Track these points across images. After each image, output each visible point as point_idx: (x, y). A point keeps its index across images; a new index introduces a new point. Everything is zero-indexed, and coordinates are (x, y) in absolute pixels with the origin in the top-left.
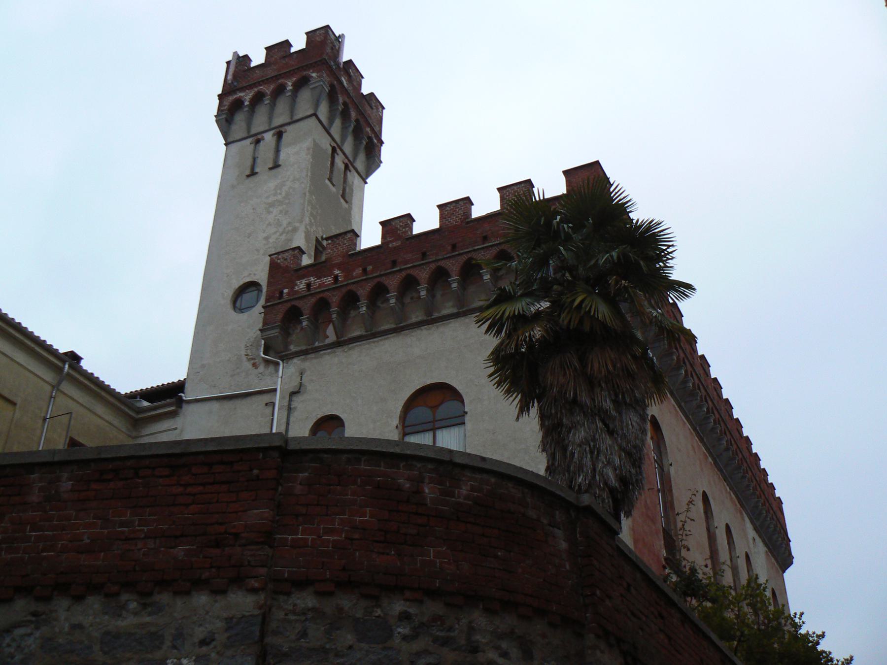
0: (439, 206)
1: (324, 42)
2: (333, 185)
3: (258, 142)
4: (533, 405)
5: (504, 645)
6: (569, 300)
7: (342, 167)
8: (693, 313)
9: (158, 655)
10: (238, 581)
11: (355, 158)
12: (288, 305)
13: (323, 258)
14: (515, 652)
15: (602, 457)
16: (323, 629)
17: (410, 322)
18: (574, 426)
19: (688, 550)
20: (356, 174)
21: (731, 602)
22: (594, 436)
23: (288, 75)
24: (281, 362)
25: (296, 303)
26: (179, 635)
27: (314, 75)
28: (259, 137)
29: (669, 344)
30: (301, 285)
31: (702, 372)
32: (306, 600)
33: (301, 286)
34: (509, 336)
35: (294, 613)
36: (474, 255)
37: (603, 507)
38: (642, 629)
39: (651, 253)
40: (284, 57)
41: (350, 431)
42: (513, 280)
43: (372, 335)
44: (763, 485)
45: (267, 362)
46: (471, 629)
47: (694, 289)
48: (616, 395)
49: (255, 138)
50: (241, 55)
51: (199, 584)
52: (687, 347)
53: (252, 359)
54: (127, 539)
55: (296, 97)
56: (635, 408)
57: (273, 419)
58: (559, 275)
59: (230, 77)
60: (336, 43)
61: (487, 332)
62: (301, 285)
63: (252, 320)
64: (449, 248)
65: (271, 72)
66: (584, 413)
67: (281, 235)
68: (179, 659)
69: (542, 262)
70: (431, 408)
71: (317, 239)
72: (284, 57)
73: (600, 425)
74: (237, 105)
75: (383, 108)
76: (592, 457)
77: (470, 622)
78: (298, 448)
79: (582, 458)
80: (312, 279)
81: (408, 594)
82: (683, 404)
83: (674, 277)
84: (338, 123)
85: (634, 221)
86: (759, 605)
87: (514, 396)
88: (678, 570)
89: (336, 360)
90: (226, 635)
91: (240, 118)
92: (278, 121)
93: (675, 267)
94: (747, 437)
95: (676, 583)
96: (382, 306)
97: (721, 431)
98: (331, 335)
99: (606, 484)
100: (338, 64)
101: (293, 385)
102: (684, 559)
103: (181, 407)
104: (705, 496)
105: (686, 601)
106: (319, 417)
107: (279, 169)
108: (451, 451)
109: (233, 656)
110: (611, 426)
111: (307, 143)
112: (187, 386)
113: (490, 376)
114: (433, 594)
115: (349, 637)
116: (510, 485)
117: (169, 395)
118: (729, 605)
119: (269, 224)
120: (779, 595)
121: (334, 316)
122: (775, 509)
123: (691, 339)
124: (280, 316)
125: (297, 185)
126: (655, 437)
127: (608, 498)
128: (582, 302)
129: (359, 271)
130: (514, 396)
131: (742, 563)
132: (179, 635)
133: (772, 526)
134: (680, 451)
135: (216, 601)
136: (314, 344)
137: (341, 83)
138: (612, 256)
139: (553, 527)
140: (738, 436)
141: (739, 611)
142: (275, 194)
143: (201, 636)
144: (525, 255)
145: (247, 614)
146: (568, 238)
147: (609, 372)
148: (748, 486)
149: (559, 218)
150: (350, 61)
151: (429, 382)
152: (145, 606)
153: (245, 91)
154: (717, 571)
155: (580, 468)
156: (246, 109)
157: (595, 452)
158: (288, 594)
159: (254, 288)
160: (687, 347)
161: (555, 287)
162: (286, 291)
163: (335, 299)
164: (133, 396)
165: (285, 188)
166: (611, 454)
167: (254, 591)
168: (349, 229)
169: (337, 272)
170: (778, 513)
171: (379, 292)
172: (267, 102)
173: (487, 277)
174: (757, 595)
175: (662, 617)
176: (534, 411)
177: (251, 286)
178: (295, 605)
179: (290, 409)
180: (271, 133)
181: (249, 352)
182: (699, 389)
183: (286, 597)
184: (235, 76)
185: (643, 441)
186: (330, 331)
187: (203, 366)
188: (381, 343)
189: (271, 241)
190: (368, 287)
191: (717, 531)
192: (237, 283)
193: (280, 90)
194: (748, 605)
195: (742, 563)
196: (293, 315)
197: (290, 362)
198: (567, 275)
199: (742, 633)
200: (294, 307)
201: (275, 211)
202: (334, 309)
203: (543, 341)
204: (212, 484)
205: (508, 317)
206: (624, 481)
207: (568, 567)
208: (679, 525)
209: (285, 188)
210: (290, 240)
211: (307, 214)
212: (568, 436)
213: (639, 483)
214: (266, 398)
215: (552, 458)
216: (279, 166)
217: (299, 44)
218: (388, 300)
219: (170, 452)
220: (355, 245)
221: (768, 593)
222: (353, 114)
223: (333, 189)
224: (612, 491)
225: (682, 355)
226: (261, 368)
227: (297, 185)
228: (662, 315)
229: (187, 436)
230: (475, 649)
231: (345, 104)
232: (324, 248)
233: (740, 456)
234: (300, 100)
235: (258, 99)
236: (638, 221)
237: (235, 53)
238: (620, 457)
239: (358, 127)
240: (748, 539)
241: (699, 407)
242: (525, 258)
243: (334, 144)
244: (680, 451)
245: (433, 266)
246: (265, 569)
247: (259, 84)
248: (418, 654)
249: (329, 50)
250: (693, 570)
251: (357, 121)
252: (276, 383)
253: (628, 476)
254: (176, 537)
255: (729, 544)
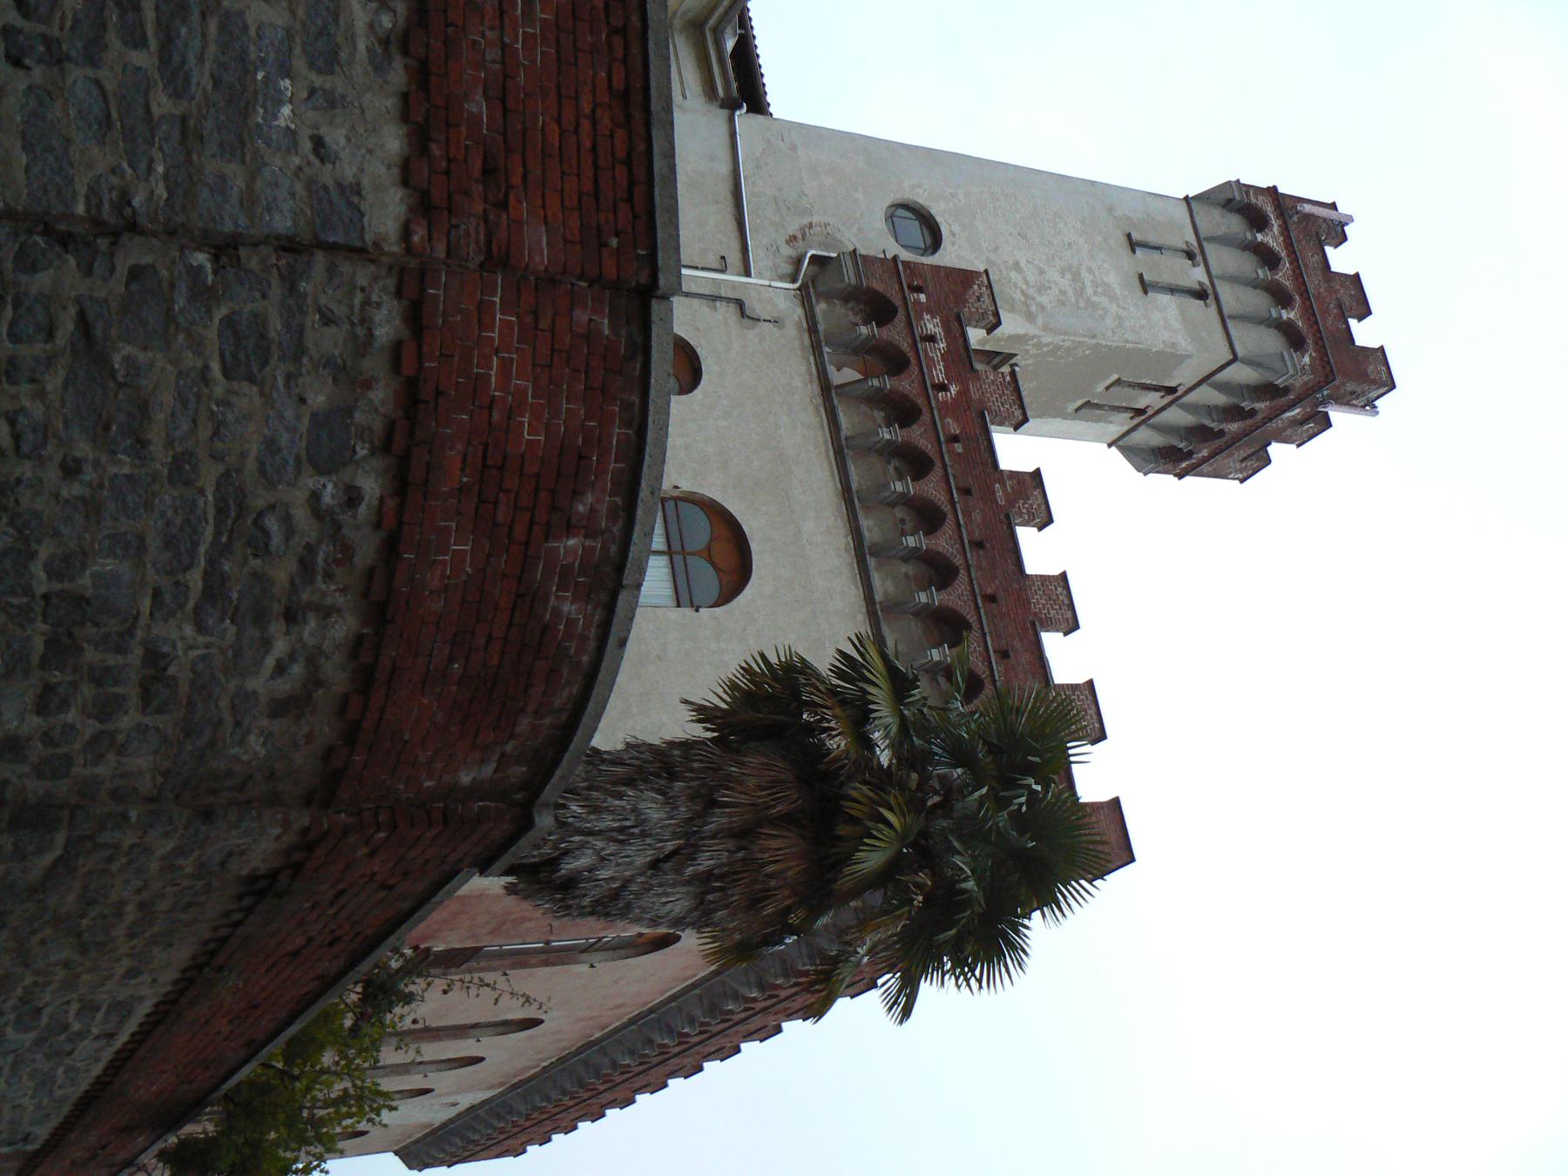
0: (1064, 575)
1: (1365, 378)
2: (1107, 388)
3: (1190, 255)
4: (708, 729)
5: (297, 669)
6: (892, 801)
7: (1140, 405)
8: (859, 1014)
9: (299, 64)
10: (424, 206)
11: (1155, 427)
12: (898, 302)
13: (978, 366)
14: (283, 687)
15: (613, 848)
16: (337, 352)
17: (861, 515)
18: (669, 801)
19: (445, 992)
20: (1126, 428)
21: (350, 1061)
22: (649, 835)
23: (1308, 312)
24: (797, 285)
25: (901, 315)
26: (332, 102)
27: (1307, 359)
28: (1199, 258)
29: (806, 974)
30: (932, 325)
31: (753, 1027)
32: (387, 325)
33: (930, 326)
34: (833, 692)
35: (366, 303)
36: (976, 633)
37: (524, 851)
38: (313, 907)
39: (969, 949)
40: (1340, 306)
41: (678, 404)
42: (929, 702)
43: (840, 450)
44: (549, 1125)
45: (798, 262)
46: (326, 612)
47: (901, 1022)
48: (721, 877)
49: (1197, 251)
50: (1346, 229)
51: (420, 137)
52: (799, 1002)
53: (804, 236)
54: (502, 13)
55: (1269, 326)
56: (696, 908)
57: (696, 268)
58: (936, 784)
59: (1307, 208)
60: (1362, 401)
61: (841, 652)
62: (932, 325)
63: (874, 237)
64: (989, 591)
65: (1314, 282)
66: (692, 819)
67: (1023, 292)
68: (291, 101)
69: (960, 754)
70: (709, 548)
71: (1013, 355)
72: (1340, 306)
73: (670, 846)
74: (1257, 220)
75: (1242, 481)
76: (613, 830)
77: (339, 611)
78: (654, 317)
79: (613, 813)
80: (942, 345)
81: (391, 504)
82: (697, 991)
83: (924, 987)
84: (1220, 399)
85: (1026, 922)
86: (344, 1109)
87: (725, 696)
88: (409, 970)
89: (797, 383)
90: (330, 183)
91: (1234, 224)
92: (1226, 292)
93: (943, 991)
94: (634, 1102)
95: (386, 967)
96: (891, 468)
97: (646, 1056)
98: (843, 376)
99: (566, 853)
100: (1324, 403)
101: (755, 306)
102: (429, 984)
103: (722, 107)
104: (534, 1023)
105: (356, 983)
106: (698, 350)
107: (1139, 292)
108: (639, 586)
109: (293, 195)
110: (667, 866)
111: (1185, 345)
112: (758, 119)
113: (762, 656)
114: (391, 548)
115: (321, 399)
116: (575, 690)
117: (744, 88)
118: (345, 1057)
119: (1042, 272)
120: (354, 1140)
121: (876, 382)
122: (510, 1142)
123: (816, 1011)
124: (878, 286)
125: (1110, 322)
126: (641, 940)
127: (542, 855)
128: (889, 825)
129: (954, 429)
130: (725, 696)
131: (415, 1081)
132: (332, 102)
133: (476, 1137)
134: (616, 982)
135: (389, 167)
136: (827, 344)
137: (1290, 407)
138: (966, 879)
139: (499, 761)
140: (637, 1086)
141: (335, 1073)
142: (1095, 283)
143: (328, 140)
144: (973, 726)
145: (366, 220)
146: (1002, 804)
147: (762, 866)
148: (548, 1099)
149: (1039, 788)
150: (1328, 425)
151: (753, 546)
152: (385, 42)
153: (1281, 234)
154: (405, 1037)
155: (596, 810)
156: (1249, 236)
157: (622, 836)
158: (399, 294)
159: (929, 241)
160: (799, 1002)
161: (914, 776)
162: (923, 297)
163: (906, 385)
164: (744, 22)
165: (1104, 301)
166: (618, 865)
167: (406, 233)
168: (1029, 414)
169: (953, 389)
170: (500, 1149)
171: (916, 463)
172: (1260, 272)
173: (936, 655)
174: (360, 1108)
175: (331, 944)
176: (698, 731)
177: (935, 239)
178: (379, 305)
179: (714, 298)
180: (1206, 281)
181: (817, 229)
182: (723, 1021)
183: (393, 290)
184: (1309, 217)
185: (637, 921)
186: (849, 375)
187: (794, 148)
188: (825, 464)
189: (1013, 274)
190: (927, 446)
191: (472, 1041)
192: (938, 211)
193: (1281, 297)
194: (345, 1090)
195: (415, 1081)
196: (879, 309)
197: (797, 302)
198: (937, 799)
199: (296, 1078)
200: (895, 311)
201: (1065, 283)
202: (888, 384)
203: (821, 752)
204: (596, 166)
205: (866, 692)
206: (569, 885)
207: (427, 784)
208: (489, 977)
209: (1104, 301)
210: (1012, 310)
211: (1058, 339)
212: (653, 789)
213: (565, 909)
214: (734, 258)
215: (616, 759)
216: (1146, 293)
217: (1364, 333)
218: (900, 480)
219: (653, 92)
220: (1001, 424)
221: (363, 1126)
222: (1233, 427)
223: (1101, 388)
224: (553, 863)
225: (783, 994)
226: (787, 251)
227: (1110, 322)
228: (859, 963)
229: (678, 117)
230: (292, 616)
231: (1253, 413)
232: (996, 368)
233: (602, 1088)
234: (1271, 332)
235: (1268, 258)
236: (1027, 927)
237: (1351, 219)
238: (612, 879)
239: (1213, 434)
240: (455, 1095)
241: (691, 1021)
242: (967, 725)
243: (1181, 390)
244: (616, 982)
245: (958, 560)
246: (443, 255)
247: (1294, 260)
248: (287, 520)
249: (1350, 387)
250: (409, 999)
251: (1221, 433)
252: (760, 275)
253: (578, 892)
254: (503, 100)
255: (449, 1060)
